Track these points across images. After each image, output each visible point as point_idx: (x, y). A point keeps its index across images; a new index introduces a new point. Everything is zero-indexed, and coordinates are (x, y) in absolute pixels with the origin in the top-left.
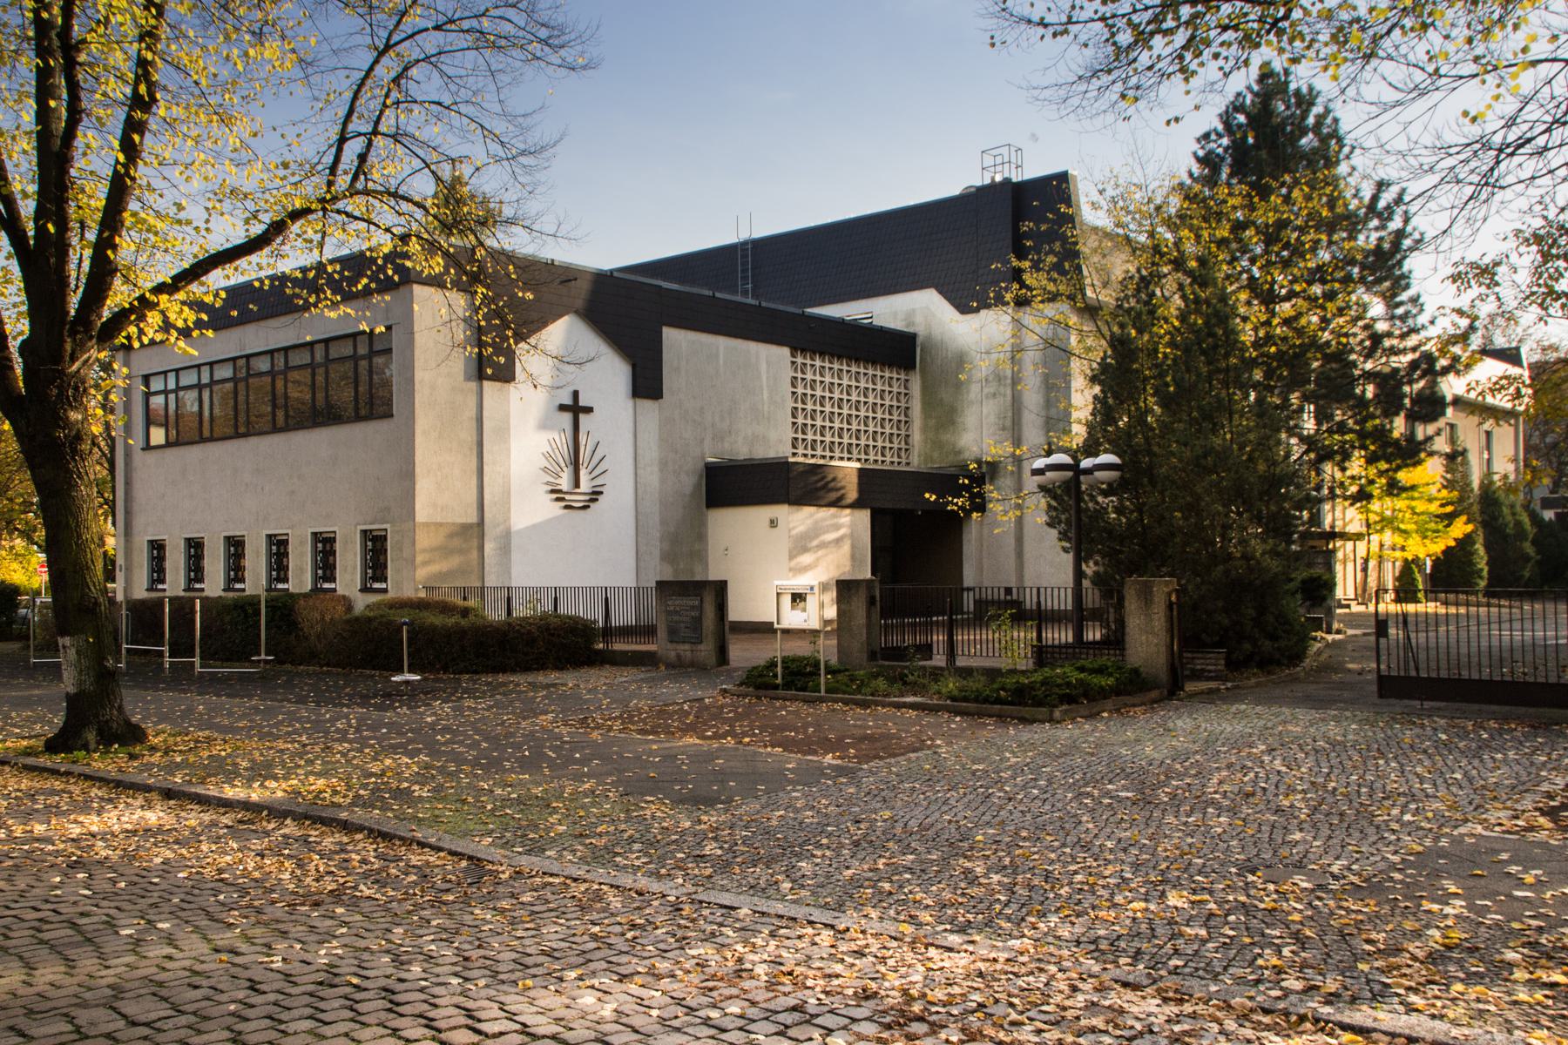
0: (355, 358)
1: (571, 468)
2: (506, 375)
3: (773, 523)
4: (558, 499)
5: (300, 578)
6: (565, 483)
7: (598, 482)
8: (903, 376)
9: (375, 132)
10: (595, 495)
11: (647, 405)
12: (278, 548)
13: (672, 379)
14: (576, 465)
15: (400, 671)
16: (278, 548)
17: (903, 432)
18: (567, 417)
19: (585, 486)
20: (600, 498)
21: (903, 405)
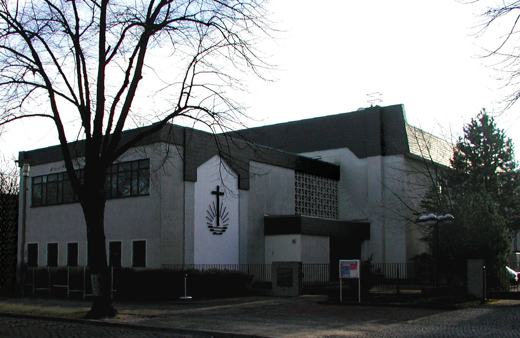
0: (58, 182)
1: (216, 217)
2: (194, 179)
3: (294, 242)
4: (211, 230)
5: (63, 260)
6: (214, 224)
7: (225, 224)
8: (335, 183)
9: (191, 87)
10: (224, 229)
11: (244, 192)
12: (53, 249)
13: (216, 187)
14: (218, 216)
15: (184, 296)
16: (53, 249)
17: (335, 206)
18: (214, 197)
19: (221, 225)
20: (227, 230)
21: (335, 195)
